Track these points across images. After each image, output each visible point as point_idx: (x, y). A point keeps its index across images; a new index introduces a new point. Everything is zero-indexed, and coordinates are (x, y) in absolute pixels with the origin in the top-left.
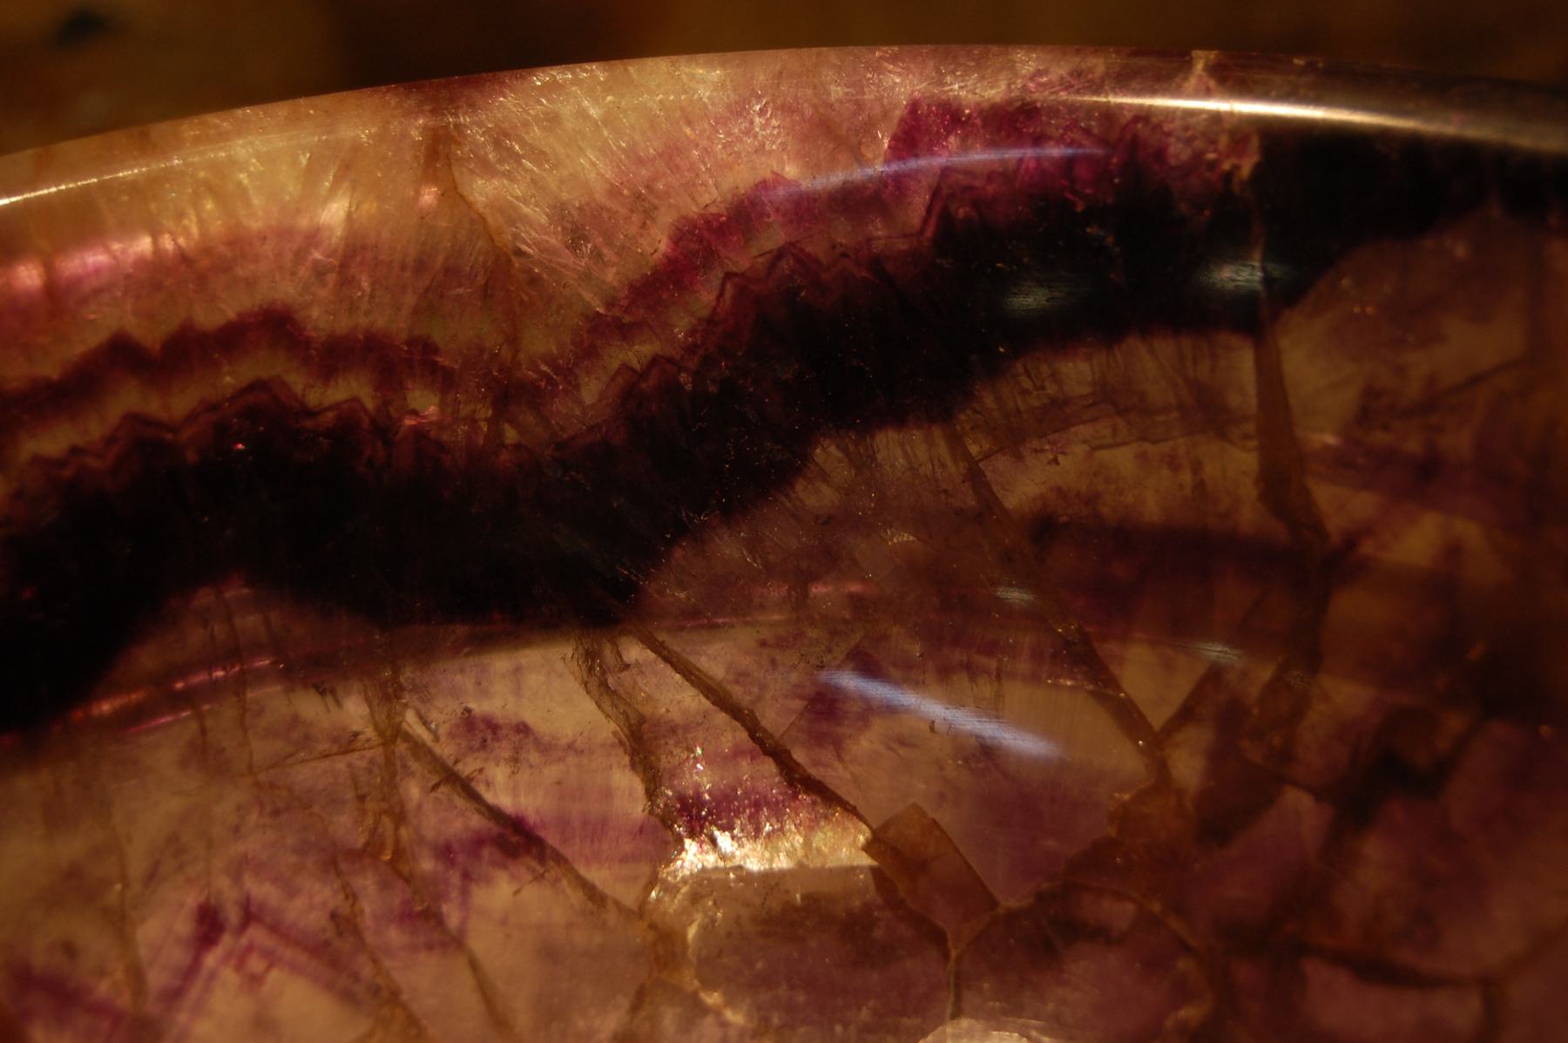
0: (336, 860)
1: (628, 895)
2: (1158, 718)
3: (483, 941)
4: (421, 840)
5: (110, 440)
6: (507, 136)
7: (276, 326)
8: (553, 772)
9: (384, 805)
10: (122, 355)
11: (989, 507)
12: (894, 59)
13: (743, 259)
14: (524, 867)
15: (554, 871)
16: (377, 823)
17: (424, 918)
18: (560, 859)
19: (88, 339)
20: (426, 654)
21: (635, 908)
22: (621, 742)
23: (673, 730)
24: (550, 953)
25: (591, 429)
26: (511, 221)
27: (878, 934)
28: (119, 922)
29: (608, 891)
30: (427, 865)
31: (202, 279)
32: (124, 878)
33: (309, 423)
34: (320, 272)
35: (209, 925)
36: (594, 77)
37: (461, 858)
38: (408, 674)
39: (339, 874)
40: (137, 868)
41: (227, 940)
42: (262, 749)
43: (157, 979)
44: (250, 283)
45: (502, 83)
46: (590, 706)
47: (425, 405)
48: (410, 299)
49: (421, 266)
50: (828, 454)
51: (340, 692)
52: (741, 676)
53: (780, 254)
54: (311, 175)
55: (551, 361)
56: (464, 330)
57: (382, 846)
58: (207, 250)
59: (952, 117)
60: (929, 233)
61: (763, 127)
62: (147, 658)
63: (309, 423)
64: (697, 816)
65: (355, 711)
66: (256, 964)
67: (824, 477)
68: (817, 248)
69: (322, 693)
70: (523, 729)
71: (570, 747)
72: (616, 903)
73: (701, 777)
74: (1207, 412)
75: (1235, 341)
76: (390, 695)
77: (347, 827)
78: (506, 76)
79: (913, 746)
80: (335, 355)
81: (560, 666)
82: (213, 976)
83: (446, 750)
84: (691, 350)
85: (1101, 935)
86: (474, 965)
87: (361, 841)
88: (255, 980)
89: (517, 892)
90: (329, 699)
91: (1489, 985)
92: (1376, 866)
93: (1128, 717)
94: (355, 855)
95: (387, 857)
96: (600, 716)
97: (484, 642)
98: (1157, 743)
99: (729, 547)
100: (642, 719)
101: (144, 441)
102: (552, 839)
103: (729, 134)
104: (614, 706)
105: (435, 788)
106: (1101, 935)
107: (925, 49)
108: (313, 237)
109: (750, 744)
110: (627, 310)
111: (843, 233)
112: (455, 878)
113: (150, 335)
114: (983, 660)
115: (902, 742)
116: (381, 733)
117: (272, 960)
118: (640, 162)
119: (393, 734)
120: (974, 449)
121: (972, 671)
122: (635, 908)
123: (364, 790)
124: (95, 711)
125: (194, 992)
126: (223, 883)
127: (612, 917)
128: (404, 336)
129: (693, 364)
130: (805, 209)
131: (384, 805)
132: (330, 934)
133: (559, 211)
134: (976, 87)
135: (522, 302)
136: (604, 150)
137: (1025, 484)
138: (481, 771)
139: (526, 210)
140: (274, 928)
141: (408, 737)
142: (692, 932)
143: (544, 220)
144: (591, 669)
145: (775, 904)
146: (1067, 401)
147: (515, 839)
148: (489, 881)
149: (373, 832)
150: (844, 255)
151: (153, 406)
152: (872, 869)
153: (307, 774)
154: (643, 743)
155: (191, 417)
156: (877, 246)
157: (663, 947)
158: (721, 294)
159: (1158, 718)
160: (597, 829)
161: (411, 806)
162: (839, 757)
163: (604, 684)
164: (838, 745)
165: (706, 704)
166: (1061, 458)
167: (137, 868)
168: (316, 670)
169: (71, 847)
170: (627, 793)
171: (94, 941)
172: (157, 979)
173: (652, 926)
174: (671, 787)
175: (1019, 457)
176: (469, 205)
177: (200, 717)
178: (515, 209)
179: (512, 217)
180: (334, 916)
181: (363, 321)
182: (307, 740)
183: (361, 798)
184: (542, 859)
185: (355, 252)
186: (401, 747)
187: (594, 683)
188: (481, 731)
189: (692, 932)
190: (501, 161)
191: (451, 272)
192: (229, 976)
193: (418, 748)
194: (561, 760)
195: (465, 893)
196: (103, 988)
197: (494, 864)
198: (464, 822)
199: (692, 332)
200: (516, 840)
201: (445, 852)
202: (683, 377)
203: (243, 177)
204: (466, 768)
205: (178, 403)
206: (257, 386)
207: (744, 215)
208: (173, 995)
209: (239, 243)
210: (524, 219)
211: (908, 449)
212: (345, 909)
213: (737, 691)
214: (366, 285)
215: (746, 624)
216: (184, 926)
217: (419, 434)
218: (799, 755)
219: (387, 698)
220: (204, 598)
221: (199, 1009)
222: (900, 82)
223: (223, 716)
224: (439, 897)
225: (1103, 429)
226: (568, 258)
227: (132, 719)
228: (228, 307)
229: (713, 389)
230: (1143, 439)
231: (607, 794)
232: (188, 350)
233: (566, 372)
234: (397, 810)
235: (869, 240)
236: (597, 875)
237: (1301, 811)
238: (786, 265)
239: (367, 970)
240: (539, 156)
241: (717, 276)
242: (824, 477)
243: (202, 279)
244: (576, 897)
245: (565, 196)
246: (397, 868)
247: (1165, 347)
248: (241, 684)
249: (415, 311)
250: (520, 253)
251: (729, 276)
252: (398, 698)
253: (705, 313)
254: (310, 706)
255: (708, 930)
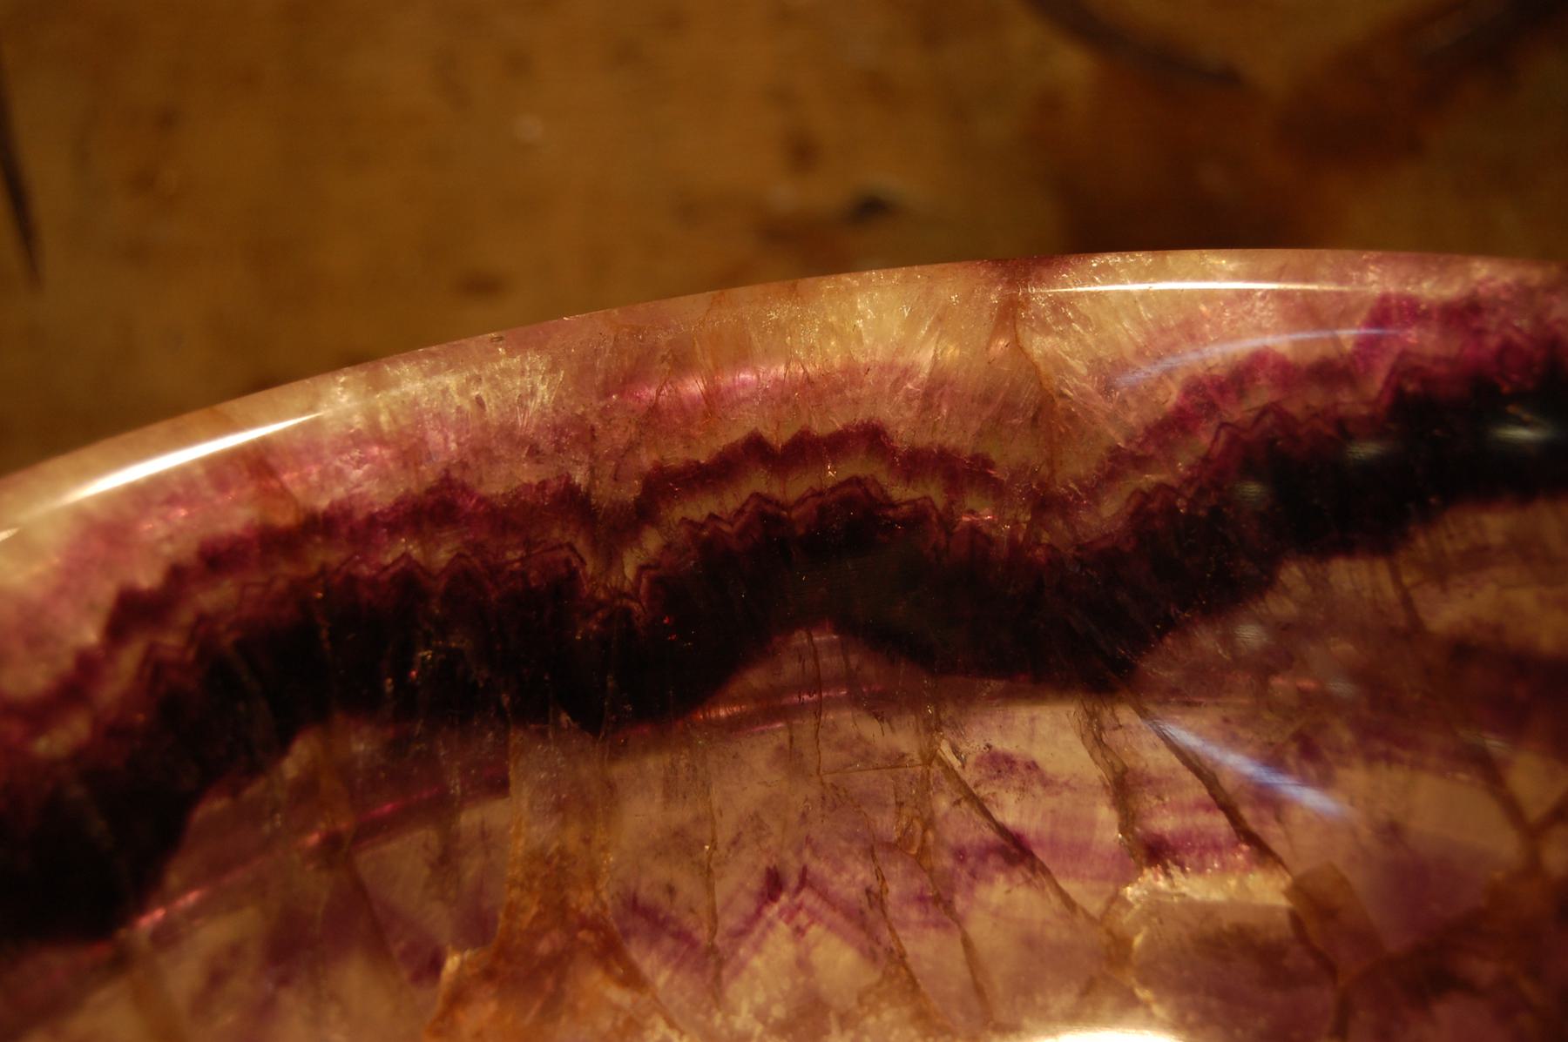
0: (874, 848)
1: (1095, 906)
2: (1535, 812)
3: (980, 928)
4: (940, 841)
5: (740, 512)
6: (1062, 304)
7: (873, 437)
8: (1051, 802)
9: (917, 812)
10: (756, 448)
11: (1415, 630)
12: (1377, 262)
13: (1239, 412)
14: (1019, 874)
15: (1041, 880)
16: (910, 824)
17: (940, 904)
18: (1045, 871)
19: (733, 435)
20: (967, 699)
21: (1098, 917)
22: (1105, 786)
23: (1150, 781)
24: (1030, 942)
25: (1105, 537)
26: (1058, 370)
28: (707, 874)
29: (1078, 900)
30: (947, 862)
31: (820, 397)
32: (713, 841)
33: (890, 513)
34: (909, 399)
35: (773, 884)
36: (1138, 261)
37: (971, 860)
38: (949, 712)
39: (874, 858)
40: (725, 834)
41: (784, 899)
42: (829, 757)
43: (729, 921)
44: (856, 402)
45: (1067, 264)
46: (1083, 753)
47: (981, 511)
48: (974, 425)
49: (986, 400)
50: (1292, 574)
51: (895, 719)
53: (1264, 411)
54: (913, 322)
55: (1077, 481)
56: (1012, 453)
57: (912, 843)
58: (826, 377)
59: (1411, 311)
61: (1262, 309)
62: (756, 679)
63: (890, 513)
64: (1157, 852)
65: (903, 738)
66: (802, 918)
67: (1287, 591)
68: (1295, 408)
69: (881, 720)
70: (1032, 766)
71: (1066, 784)
72: (1084, 911)
73: (1166, 823)
76: (933, 727)
77: (887, 824)
78: (1072, 260)
80: (916, 463)
81: (1065, 720)
82: (771, 925)
83: (969, 776)
84: (1189, 481)
85: (1468, 987)
86: (967, 943)
87: (896, 836)
88: (799, 931)
89: (1009, 892)
90: (886, 725)
93: (1512, 809)
94: (890, 847)
95: (914, 852)
96: (1092, 763)
97: (1012, 696)
98: (1533, 833)
99: (1206, 640)
100: (1125, 770)
101: (766, 515)
102: (1040, 854)
103: (1233, 313)
104: (1104, 756)
105: (958, 802)
106: (1468, 987)
107: (1402, 255)
108: (907, 372)
109: (1209, 800)
110: (1140, 445)
111: (1316, 397)
112: (964, 873)
113: (779, 436)
114: (1397, 751)
116: (923, 757)
117: (814, 917)
118: (1163, 331)
119: (931, 757)
121: (1389, 759)
122: (1098, 917)
123: (904, 799)
124: (713, 715)
125: (758, 930)
126: (789, 855)
127: (1080, 920)
128: (969, 453)
129: (1190, 493)
130: (1287, 373)
131: (917, 812)
132: (865, 904)
133: (1096, 365)
134: (1433, 288)
135: (1061, 434)
136: (1139, 321)
137: (1450, 611)
138: (994, 794)
139: (1072, 362)
140: (824, 895)
141: (941, 762)
143: (1084, 371)
144: (1090, 724)
146: (1486, 548)
147: (1014, 851)
148: (990, 881)
149: (904, 832)
150: (1316, 415)
151: (775, 490)
153: (863, 780)
154: (1125, 787)
155: (802, 500)
156: (1341, 410)
157: (1116, 952)
158: (1216, 439)
160: (1079, 852)
161: (939, 815)
162: (1278, 819)
163: (1098, 741)
165: (1177, 762)
167: (725, 834)
168: (880, 705)
169: (682, 814)
171: (688, 886)
172: (729, 921)
173: (1110, 932)
174: (1141, 827)
175: (1444, 590)
176: (1027, 356)
177: (790, 728)
178: (1064, 361)
179: (1061, 367)
180: (868, 891)
181: (939, 438)
182: (866, 757)
183: (900, 804)
184: (1033, 869)
185: (936, 389)
186: (936, 769)
187: (1090, 737)
188: (1000, 764)
190: (1057, 323)
191: (1008, 407)
192: (783, 927)
193: (948, 769)
194: (1058, 794)
195: (971, 887)
196: (689, 921)
197: (998, 869)
198: (975, 833)
199: (1190, 467)
200: (1015, 851)
201: (960, 854)
202: (1180, 502)
203: (859, 323)
204: (982, 792)
205: (795, 487)
206: (856, 481)
207: (1241, 376)
208: (740, 934)
209: (853, 373)
210: (1071, 370)
212: (876, 888)
214: (945, 411)
215: (1217, 704)
216: (755, 883)
217: (974, 529)
218: (1246, 813)
219: (929, 730)
220: (800, 638)
221: (757, 948)
222: (1376, 279)
223: (806, 725)
224: (951, 889)
226: (1099, 401)
227: (734, 726)
228: (837, 421)
229: (1202, 513)
231: (1092, 824)
232: (805, 449)
233: (1093, 491)
234: (926, 816)
235: (1336, 404)
236: (1071, 887)
238: (1269, 420)
239: (886, 936)
240: (1085, 321)
241: (1212, 425)
242: (1287, 591)
243: (820, 397)
244: (1055, 902)
245: (1102, 353)
246: (921, 860)
248: (818, 709)
249: (979, 434)
250: (1063, 396)
251: (1223, 425)
252: (938, 730)
253: (1202, 453)
254: (871, 729)
255: (1150, 943)
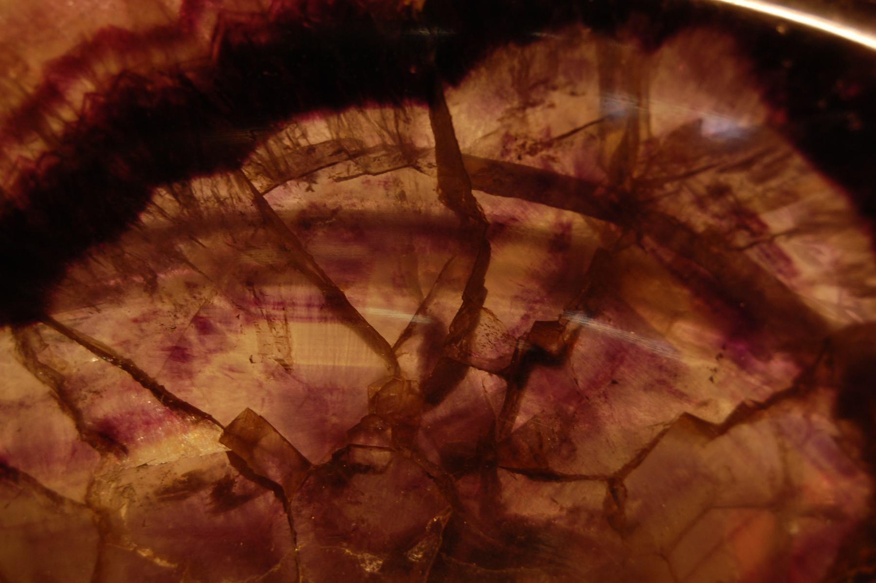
18: (29, 479)
21: (84, 503)
27: (236, 490)
52: (125, 343)
60: (216, 51)
74: (408, 155)
75: (418, 109)
79: (242, 372)
91: (614, 482)
92: (530, 409)
93: (371, 336)
98: (390, 353)
100: (63, 379)
104: (45, 374)
115: (232, 370)
120: (257, 185)
122: (84, 503)
142: (123, 512)
145: (168, 482)
152: (228, 453)
159: (392, 341)
164: (190, 374)
166: (314, 186)
170: (63, 427)
189: (123, 512)
211: (310, 266)
213: (119, 350)
218: (168, 386)
225: (340, 169)
230: (367, 173)
236: (55, 485)
237: (482, 382)
244: (41, 499)
247: (373, 114)
